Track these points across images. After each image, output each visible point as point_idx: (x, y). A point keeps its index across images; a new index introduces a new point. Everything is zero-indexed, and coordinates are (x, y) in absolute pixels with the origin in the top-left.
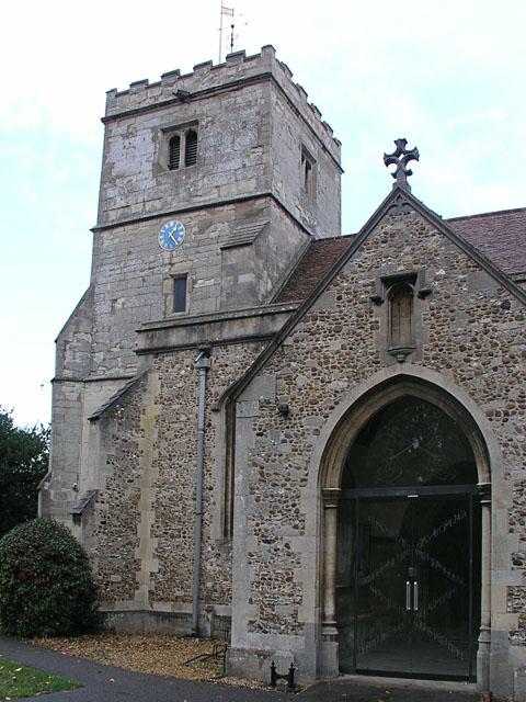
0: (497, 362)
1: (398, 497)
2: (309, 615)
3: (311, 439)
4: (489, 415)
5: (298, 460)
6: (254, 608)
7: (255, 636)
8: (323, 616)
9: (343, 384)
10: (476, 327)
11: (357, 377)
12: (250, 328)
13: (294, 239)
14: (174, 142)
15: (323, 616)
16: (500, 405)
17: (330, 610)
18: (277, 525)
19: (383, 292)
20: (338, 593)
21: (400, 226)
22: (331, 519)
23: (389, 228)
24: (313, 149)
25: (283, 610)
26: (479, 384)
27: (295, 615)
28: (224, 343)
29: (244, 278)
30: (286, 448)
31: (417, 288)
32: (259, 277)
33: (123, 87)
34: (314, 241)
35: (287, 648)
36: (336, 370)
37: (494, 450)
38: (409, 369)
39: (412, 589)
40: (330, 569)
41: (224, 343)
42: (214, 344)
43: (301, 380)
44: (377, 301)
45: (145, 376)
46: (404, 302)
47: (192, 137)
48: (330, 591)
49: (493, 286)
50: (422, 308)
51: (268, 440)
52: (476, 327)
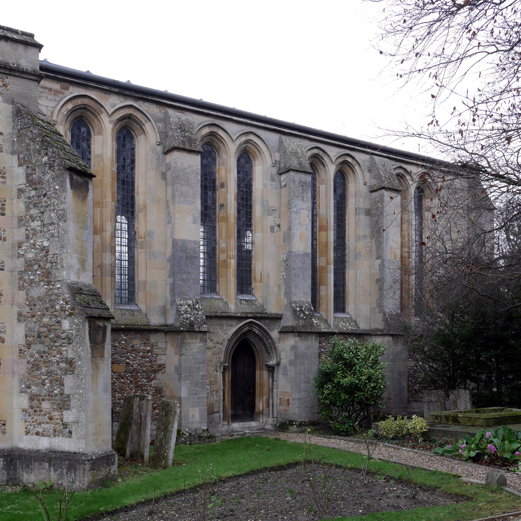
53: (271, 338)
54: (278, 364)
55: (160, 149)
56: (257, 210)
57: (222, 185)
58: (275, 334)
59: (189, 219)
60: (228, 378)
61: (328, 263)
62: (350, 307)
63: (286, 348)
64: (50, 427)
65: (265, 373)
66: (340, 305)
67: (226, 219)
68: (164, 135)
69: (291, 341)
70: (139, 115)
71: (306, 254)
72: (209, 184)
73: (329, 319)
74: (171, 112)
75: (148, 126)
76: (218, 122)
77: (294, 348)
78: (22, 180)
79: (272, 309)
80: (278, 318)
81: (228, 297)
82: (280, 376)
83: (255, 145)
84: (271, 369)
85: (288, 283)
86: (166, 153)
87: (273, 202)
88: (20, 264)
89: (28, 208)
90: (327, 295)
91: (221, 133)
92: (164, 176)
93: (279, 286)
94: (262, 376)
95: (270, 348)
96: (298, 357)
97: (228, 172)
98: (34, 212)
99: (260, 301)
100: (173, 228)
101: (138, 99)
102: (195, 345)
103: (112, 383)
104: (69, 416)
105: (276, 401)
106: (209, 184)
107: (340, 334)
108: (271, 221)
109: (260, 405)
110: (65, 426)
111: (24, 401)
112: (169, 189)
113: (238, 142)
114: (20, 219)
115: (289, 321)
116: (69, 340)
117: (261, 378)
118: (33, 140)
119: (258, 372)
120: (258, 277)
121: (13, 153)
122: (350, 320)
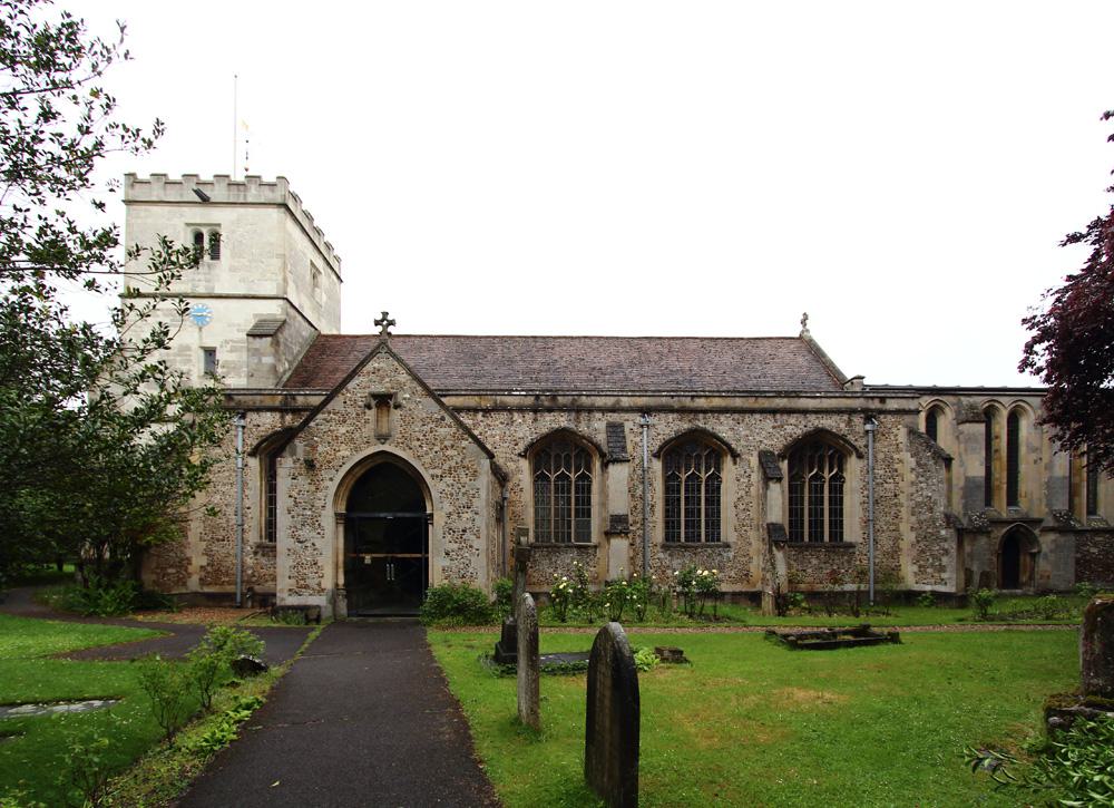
2: (328, 584)
3: (329, 483)
4: (432, 476)
6: (293, 581)
9: (348, 453)
11: (357, 449)
13: (306, 332)
16: (439, 472)
17: (341, 581)
18: (305, 533)
19: (373, 403)
20: (346, 573)
21: (382, 365)
22: (341, 529)
23: (376, 365)
25: (312, 583)
26: (427, 459)
27: (319, 584)
34: (320, 335)
38: (387, 447)
40: (341, 558)
46: (385, 409)
47: (215, 238)
48: (341, 571)
53: (1033, 534)
54: (1039, 552)
55: (955, 422)
56: (1023, 450)
57: (997, 437)
58: (1037, 532)
59: (977, 463)
60: (1000, 560)
61: (1081, 481)
62: (1101, 511)
63: (1047, 541)
64: (933, 581)
65: (1028, 559)
66: (1092, 510)
67: (1000, 459)
68: (958, 413)
69: (1052, 536)
70: (942, 404)
71: (1064, 478)
72: (989, 437)
73: (1083, 520)
74: (962, 398)
75: (947, 410)
76: (995, 398)
77: (1054, 541)
78: (914, 465)
79: (1035, 515)
80: (1040, 521)
81: (1001, 508)
82: (1041, 560)
83: (1023, 408)
84: (1033, 556)
85: (1049, 498)
86: (958, 424)
87: (1036, 444)
88: (912, 504)
89: (917, 477)
90: (1080, 504)
91: (997, 404)
92: (958, 437)
93: (1041, 500)
94: (1025, 560)
95: (1034, 541)
96: (1058, 547)
97: (1001, 427)
98: (921, 479)
99: (1025, 510)
100: (965, 470)
101: (940, 395)
102: (983, 540)
103: (1078, 562)
104: (944, 576)
105: (1037, 577)
106: (989, 437)
107: (1092, 530)
108: (1034, 456)
109: (1024, 579)
110: (942, 580)
111: (915, 568)
112: (962, 446)
113: (1009, 409)
114: (912, 483)
115: (1050, 522)
116: (945, 540)
117: (1025, 560)
118: (921, 445)
119: (1022, 558)
120: (1023, 494)
121: (907, 451)
122: (1102, 520)
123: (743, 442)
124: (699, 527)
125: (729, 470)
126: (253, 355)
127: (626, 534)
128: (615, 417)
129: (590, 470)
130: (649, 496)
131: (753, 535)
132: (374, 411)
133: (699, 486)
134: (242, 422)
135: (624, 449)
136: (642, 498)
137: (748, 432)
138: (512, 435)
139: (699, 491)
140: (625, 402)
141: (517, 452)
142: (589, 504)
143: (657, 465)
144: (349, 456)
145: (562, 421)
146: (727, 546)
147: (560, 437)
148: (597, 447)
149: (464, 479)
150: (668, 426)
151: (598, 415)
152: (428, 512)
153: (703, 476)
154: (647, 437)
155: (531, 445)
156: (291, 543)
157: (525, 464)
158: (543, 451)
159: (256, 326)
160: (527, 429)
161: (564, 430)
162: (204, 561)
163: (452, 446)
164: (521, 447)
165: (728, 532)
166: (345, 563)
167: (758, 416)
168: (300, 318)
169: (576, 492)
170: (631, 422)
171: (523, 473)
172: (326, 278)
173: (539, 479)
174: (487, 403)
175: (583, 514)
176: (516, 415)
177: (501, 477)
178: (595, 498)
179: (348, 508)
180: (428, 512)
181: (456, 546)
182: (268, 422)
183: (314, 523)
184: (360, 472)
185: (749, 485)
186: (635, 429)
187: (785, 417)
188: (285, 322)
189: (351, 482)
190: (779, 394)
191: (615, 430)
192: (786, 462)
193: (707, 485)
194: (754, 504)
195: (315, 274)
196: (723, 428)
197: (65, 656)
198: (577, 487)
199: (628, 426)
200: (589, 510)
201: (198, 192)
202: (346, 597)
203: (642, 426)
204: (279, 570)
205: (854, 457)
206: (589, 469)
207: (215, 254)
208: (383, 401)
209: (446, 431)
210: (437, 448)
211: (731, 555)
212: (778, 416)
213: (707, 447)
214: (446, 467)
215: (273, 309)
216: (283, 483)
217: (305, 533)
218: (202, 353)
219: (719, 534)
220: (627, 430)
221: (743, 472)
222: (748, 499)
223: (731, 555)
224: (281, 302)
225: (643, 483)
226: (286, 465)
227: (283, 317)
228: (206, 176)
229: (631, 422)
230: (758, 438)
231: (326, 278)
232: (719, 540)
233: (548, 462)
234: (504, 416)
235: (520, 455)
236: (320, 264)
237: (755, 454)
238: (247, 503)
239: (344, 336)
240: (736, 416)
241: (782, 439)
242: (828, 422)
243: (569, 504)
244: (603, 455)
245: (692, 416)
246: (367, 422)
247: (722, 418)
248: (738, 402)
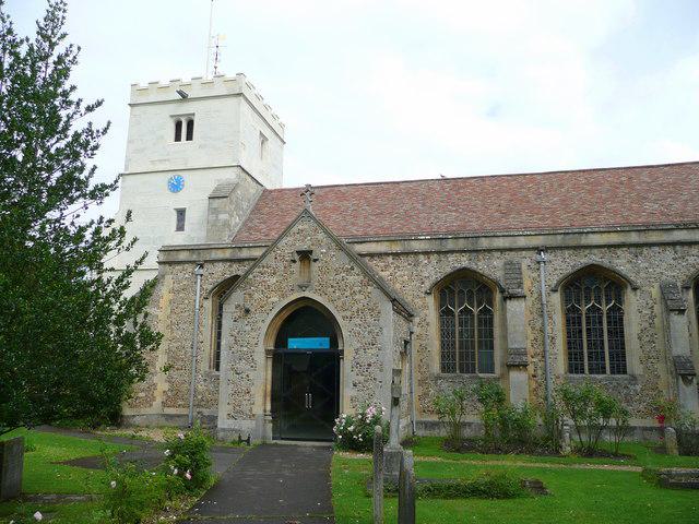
0: (347, 294)
1: (443, 345)
2: (258, 410)
3: (260, 324)
4: (343, 317)
5: (254, 334)
6: (231, 407)
7: (231, 421)
8: (265, 411)
9: (276, 299)
10: (339, 277)
11: (283, 296)
12: (227, 254)
13: (253, 190)
14: (178, 125)
15: (265, 411)
16: (349, 314)
17: (269, 407)
18: (242, 365)
19: (297, 257)
20: (273, 400)
21: (306, 227)
22: (270, 363)
23: (300, 227)
24: (267, 133)
25: (245, 409)
26: (339, 303)
27: (251, 410)
28: (213, 261)
29: (223, 217)
30: (248, 328)
31: (313, 257)
32: (231, 216)
33: (143, 84)
34: (265, 191)
35: (247, 426)
36: (271, 295)
37: (345, 332)
38: (307, 294)
39: (308, 396)
40: (269, 387)
41: (213, 261)
42: (206, 261)
43: (256, 296)
44: (294, 261)
45: (163, 276)
46: (306, 262)
47: (190, 124)
48: (269, 399)
49: (347, 260)
50: (315, 266)
51: (239, 324)
52: (339, 277)
123: (642, 275)
124: (603, 359)
125: (633, 305)
126: (213, 213)
127: (525, 366)
128: (509, 256)
129: (491, 305)
130: (548, 329)
131: (660, 368)
132: (298, 263)
133: (601, 318)
134: (201, 271)
135: (520, 285)
136: (542, 331)
137: (646, 265)
138: (416, 280)
139: (601, 323)
140: (522, 242)
141: (423, 290)
142: (492, 336)
143: (556, 298)
144: (278, 302)
145: (464, 262)
146: (634, 378)
147: (592, 272)
148: (497, 283)
149: (369, 319)
150: (563, 265)
151: (497, 254)
152: (340, 348)
153: (605, 308)
154: (544, 276)
155: (437, 284)
156: (231, 375)
157: (431, 301)
158: (447, 287)
159: (217, 189)
160: (434, 270)
161: (464, 269)
162: (166, 387)
163: (360, 292)
164: (428, 285)
165: (634, 363)
166: (273, 391)
167: (656, 249)
168: (249, 179)
169: (479, 325)
170: (526, 261)
171: (429, 311)
172: (272, 142)
173: (445, 314)
174: (397, 248)
175: (486, 345)
176: (421, 257)
177: (404, 311)
178: (497, 331)
179: (276, 345)
180: (340, 348)
181: (362, 378)
182: (220, 272)
183: (251, 359)
184: (286, 314)
185: (652, 317)
186: (533, 266)
187: (686, 248)
188: (237, 184)
189: (279, 322)
190: (678, 227)
191: (513, 269)
192: (691, 293)
193: (608, 317)
194: (660, 335)
195: (264, 139)
196: (622, 263)
197: (66, 463)
198: (480, 321)
199: (525, 264)
200: (492, 342)
201: (180, 93)
202: (272, 422)
203: (539, 263)
204: (220, 414)
205: (629, 289)
206: (491, 303)
207: (189, 137)
208: (305, 256)
209: (355, 278)
210: (347, 294)
211: (638, 387)
212: (678, 248)
213: (606, 279)
214: (355, 309)
215: (230, 176)
216: (227, 323)
217: (242, 365)
218: (175, 213)
219: (625, 366)
220: (524, 267)
221: (644, 305)
222: (531, 321)
223: (638, 387)
224: (235, 169)
225: (542, 316)
226: (230, 309)
227: (236, 181)
228: (186, 79)
229: (526, 261)
230: (658, 270)
231: (272, 142)
232: (625, 372)
233: (452, 299)
234: (411, 258)
235: (426, 293)
236: (267, 133)
237: (657, 285)
238: (201, 338)
239: (285, 190)
240: (633, 250)
241: (685, 270)
242: (595, 258)
243: (473, 337)
244: (502, 291)
245: (588, 251)
246: (292, 273)
247: (619, 252)
248: (634, 238)
